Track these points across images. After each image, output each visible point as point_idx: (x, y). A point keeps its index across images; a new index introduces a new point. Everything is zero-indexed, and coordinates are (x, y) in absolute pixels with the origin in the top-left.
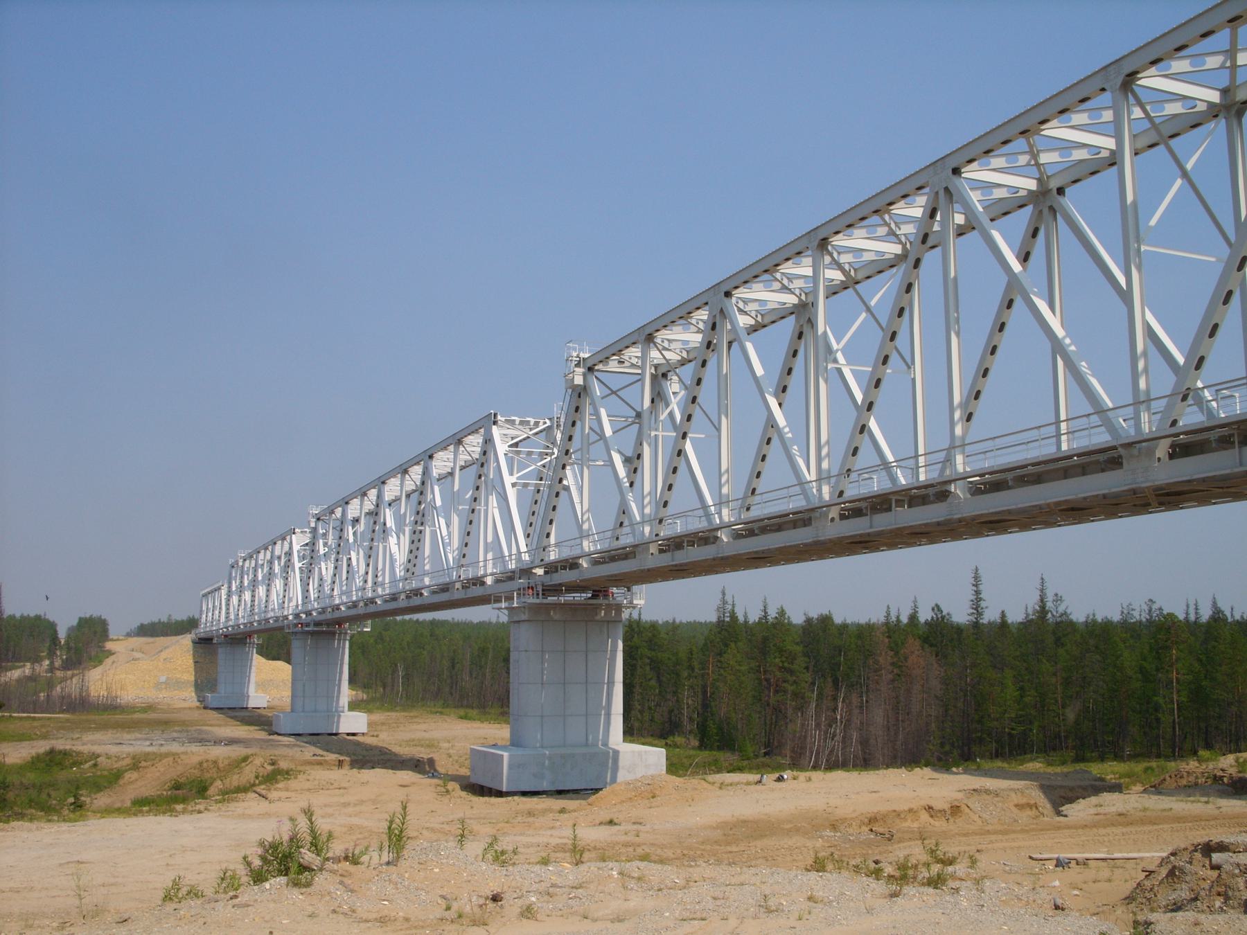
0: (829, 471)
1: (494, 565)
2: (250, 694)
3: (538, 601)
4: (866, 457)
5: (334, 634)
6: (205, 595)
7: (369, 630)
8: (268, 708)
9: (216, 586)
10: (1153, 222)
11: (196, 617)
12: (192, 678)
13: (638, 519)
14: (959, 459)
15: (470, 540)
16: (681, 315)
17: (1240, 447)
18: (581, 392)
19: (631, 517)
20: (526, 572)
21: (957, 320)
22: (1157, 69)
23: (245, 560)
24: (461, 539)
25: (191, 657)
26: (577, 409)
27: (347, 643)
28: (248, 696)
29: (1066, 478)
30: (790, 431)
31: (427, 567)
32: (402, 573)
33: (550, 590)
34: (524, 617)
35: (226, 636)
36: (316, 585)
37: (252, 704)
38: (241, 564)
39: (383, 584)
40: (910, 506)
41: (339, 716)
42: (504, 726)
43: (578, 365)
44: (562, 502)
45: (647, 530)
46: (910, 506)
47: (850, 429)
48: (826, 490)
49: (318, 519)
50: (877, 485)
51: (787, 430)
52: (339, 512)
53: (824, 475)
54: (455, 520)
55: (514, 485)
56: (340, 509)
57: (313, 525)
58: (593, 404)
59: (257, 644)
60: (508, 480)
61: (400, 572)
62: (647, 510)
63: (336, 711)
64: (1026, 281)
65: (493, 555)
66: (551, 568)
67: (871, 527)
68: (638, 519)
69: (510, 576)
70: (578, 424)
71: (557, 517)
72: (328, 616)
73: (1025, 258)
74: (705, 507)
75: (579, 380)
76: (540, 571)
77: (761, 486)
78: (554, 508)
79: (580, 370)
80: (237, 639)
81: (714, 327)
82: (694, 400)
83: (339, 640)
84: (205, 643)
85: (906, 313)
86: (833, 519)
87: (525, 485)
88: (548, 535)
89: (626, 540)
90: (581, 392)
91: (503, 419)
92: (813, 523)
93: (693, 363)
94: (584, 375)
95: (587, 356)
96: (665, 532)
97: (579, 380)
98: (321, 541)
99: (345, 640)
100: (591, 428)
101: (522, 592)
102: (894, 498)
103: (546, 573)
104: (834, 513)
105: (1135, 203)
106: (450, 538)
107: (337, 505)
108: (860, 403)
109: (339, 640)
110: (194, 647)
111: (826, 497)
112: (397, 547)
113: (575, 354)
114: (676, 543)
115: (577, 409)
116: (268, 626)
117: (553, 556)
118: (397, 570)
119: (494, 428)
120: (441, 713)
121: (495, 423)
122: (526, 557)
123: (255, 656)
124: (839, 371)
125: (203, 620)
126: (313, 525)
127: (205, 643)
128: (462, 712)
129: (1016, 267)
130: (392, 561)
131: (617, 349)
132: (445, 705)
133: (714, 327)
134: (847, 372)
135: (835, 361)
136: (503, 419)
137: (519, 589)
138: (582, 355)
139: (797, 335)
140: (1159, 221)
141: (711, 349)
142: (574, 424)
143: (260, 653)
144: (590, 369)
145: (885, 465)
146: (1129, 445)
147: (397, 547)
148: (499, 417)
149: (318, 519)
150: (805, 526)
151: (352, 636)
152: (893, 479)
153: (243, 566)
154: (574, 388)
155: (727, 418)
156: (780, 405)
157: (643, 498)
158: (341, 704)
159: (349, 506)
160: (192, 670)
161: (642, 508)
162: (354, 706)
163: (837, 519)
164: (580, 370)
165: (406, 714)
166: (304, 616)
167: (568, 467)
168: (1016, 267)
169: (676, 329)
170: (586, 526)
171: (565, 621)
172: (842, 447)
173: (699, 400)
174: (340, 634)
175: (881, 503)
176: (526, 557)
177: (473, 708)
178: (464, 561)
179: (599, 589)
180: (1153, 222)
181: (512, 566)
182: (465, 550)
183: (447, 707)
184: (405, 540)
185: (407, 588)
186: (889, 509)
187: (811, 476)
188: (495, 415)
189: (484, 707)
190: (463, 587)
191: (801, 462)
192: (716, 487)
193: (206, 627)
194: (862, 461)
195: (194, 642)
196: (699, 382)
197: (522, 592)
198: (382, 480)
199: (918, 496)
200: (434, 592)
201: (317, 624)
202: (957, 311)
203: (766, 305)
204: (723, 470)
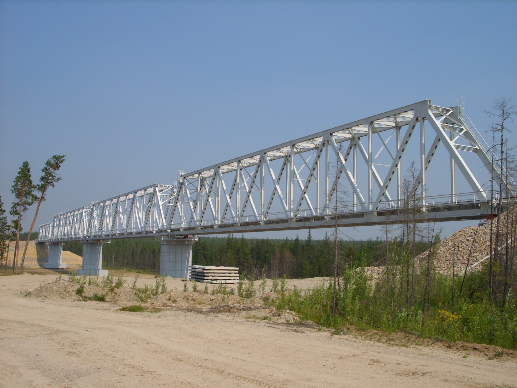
0: (293, 208)
1: (156, 228)
2: (60, 263)
3: (168, 239)
4: (303, 206)
5: (97, 243)
6: (42, 227)
7: (110, 242)
8: (67, 268)
9: (48, 223)
10: (375, 158)
11: (38, 232)
12: (36, 257)
13: (234, 215)
14: (328, 210)
15: (129, 222)
16: (209, 169)
17: (390, 215)
18: (182, 184)
19: (194, 220)
20: (166, 231)
21: (329, 174)
22: (387, 119)
23: (61, 216)
24: (127, 222)
25: (35, 249)
26: (181, 188)
27: (102, 247)
28: (59, 264)
29: (466, 209)
30: (283, 196)
31: (117, 228)
32: (126, 227)
33: (172, 236)
34: (165, 243)
35: (52, 242)
36: (74, 230)
37: (61, 267)
38: (59, 217)
39: (93, 233)
40: (315, 220)
41: (99, 271)
42: (153, 275)
43: (181, 176)
44: (176, 212)
45: (198, 223)
46: (315, 220)
47: (268, 203)
48: (292, 214)
49: (94, 206)
50: (306, 214)
51: (230, 203)
52: (102, 204)
53: (292, 210)
54: (126, 216)
55: (162, 205)
56: (81, 210)
57: (92, 207)
58: (185, 186)
59: (63, 245)
60: (161, 203)
61: (110, 228)
62: (198, 218)
63: (98, 269)
64: (346, 166)
65: (156, 225)
66: (173, 230)
67: (304, 225)
68: (234, 215)
69: (161, 231)
70: (181, 192)
71: (175, 216)
72: (56, 241)
73: (346, 160)
74: (255, 215)
75: (181, 181)
76: (169, 231)
77: (270, 211)
78: (174, 214)
79: (182, 178)
80: (55, 244)
81: (215, 175)
82: (254, 182)
83: (99, 246)
84: (41, 245)
85: (316, 169)
86: (239, 226)
87: (165, 205)
88: (172, 221)
89: (193, 225)
90: (182, 184)
91: (159, 185)
92: (364, 216)
93: (409, 125)
94: (183, 179)
95: (184, 174)
96: (202, 224)
97: (181, 181)
98: (75, 218)
99: (101, 246)
100: (184, 193)
101: (164, 236)
102: (310, 218)
103: (171, 231)
104: (239, 225)
105: (371, 152)
106: (124, 221)
107: (102, 202)
108: (303, 189)
109: (99, 246)
110: (36, 246)
111: (292, 216)
112: (109, 221)
113: (180, 174)
114: (204, 228)
115: (181, 188)
116: (64, 240)
117: (173, 227)
118: (109, 228)
119: (157, 188)
120: (130, 271)
121: (157, 187)
122: (165, 227)
123: (62, 251)
124: (298, 180)
125: (41, 235)
126: (92, 207)
127: (41, 245)
128: (137, 271)
129: (344, 162)
130: (95, 227)
131: (192, 174)
132: (131, 268)
133: (215, 175)
134: (300, 181)
135: (297, 178)
136: (159, 185)
137: (164, 235)
138: (182, 174)
139: (254, 177)
140: (377, 157)
141: (417, 121)
142: (180, 192)
143: (64, 250)
144: (185, 178)
145: (310, 209)
146: (366, 213)
147: (139, 215)
148: (158, 185)
149: (94, 206)
150: (285, 223)
151: (104, 244)
152: (312, 213)
153: (60, 218)
154: (180, 183)
155: (239, 194)
156: (230, 198)
157: (197, 215)
158: (99, 267)
159: (120, 199)
160: (36, 254)
161: (197, 217)
162: (104, 267)
163: (200, 229)
164: (182, 178)
165: (118, 271)
166: (87, 237)
167: (178, 203)
168: (344, 162)
169: (275, 151)
170: (182, 220)
171: (176, 245)
172: (297, 203)
173: (255, 182)
174: (99, 243)
175: (307, 219)
176: (165, 227)
177: (140, 269)
178: (146, 225)
179: (186, 236)
180: (375, 158)
181: (160, 228)
182: (128, 225)
183: (131, 269)
184: (111, 219)
185: (112, 233)
186: (249, 226)
187: (287, 208)
188: (157, 184)
189: (144, 269)
190: (146, 233)
191: (285, 205)
192: (259, 209)
193: (42, 238)
194: (301, 208)
195: (36, 244)
196: (255, 177)
197: (164, 236)
198: (119, 197)
199: (317, 218)
200: (119, 235)
201: (93, 240)
202: (329, 171)
203: (382, 126)
204: (237, 207)
